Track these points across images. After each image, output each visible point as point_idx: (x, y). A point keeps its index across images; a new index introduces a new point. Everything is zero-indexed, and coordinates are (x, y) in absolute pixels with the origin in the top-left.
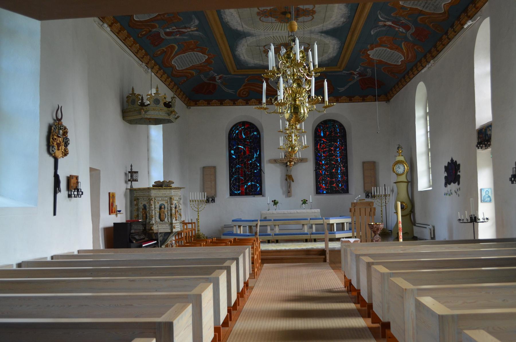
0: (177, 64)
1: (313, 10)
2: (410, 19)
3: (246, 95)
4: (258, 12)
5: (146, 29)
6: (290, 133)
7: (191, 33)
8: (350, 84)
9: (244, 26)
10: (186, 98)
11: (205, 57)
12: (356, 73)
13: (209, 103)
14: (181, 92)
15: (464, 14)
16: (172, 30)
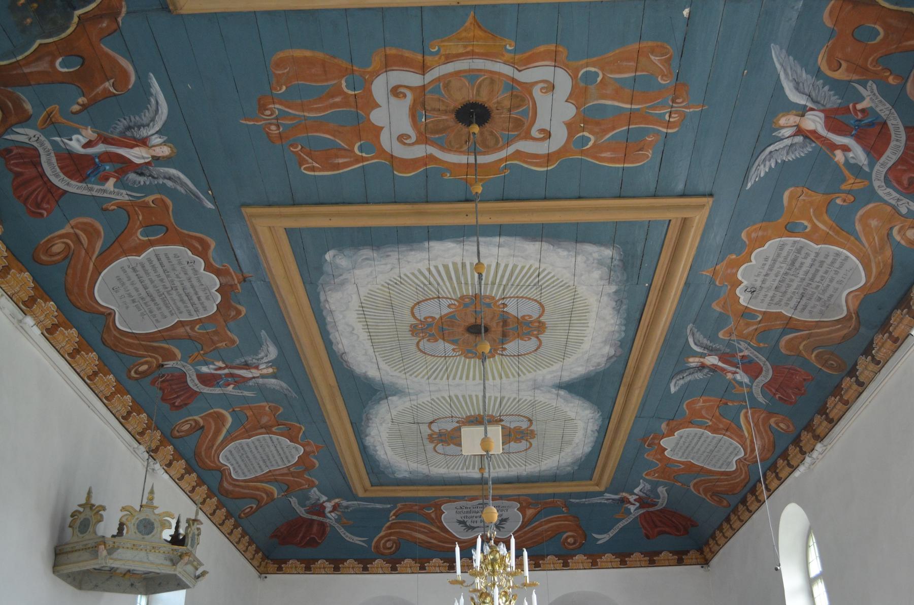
0: (232, 465)
1: (540, 322)
2: (762, 345)
3: (393, 549)
4: (412, 325)
5: (149, 359)
6: (486, 587)
7: (261, 381)
8: (621, 525)
9: (383, 365)
10: (257, 552)
11: (297, 449)
12: (635, 497)
13: (308, 567)
14: (243, 536)
15: (899, 312)
16: (216, 370)
